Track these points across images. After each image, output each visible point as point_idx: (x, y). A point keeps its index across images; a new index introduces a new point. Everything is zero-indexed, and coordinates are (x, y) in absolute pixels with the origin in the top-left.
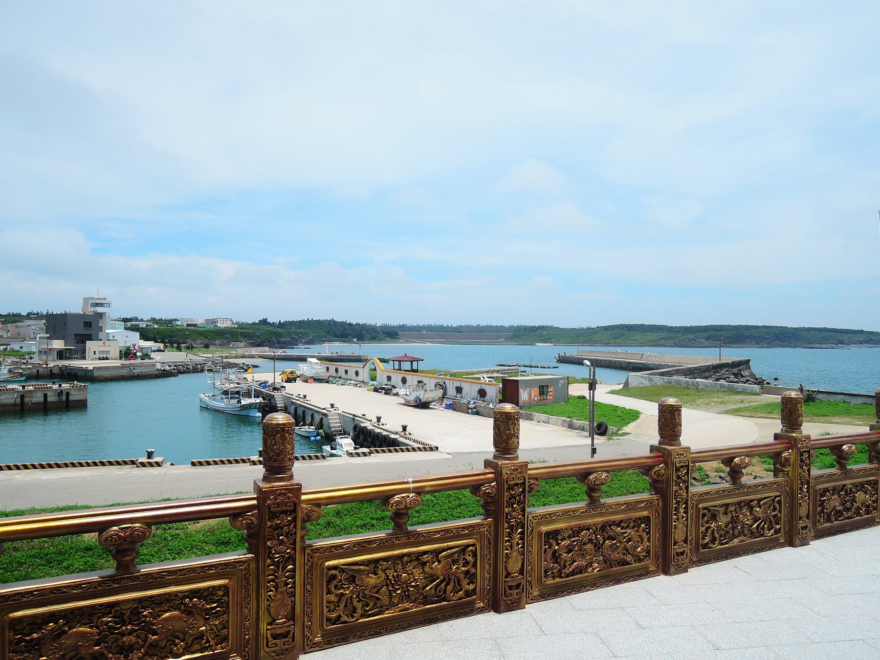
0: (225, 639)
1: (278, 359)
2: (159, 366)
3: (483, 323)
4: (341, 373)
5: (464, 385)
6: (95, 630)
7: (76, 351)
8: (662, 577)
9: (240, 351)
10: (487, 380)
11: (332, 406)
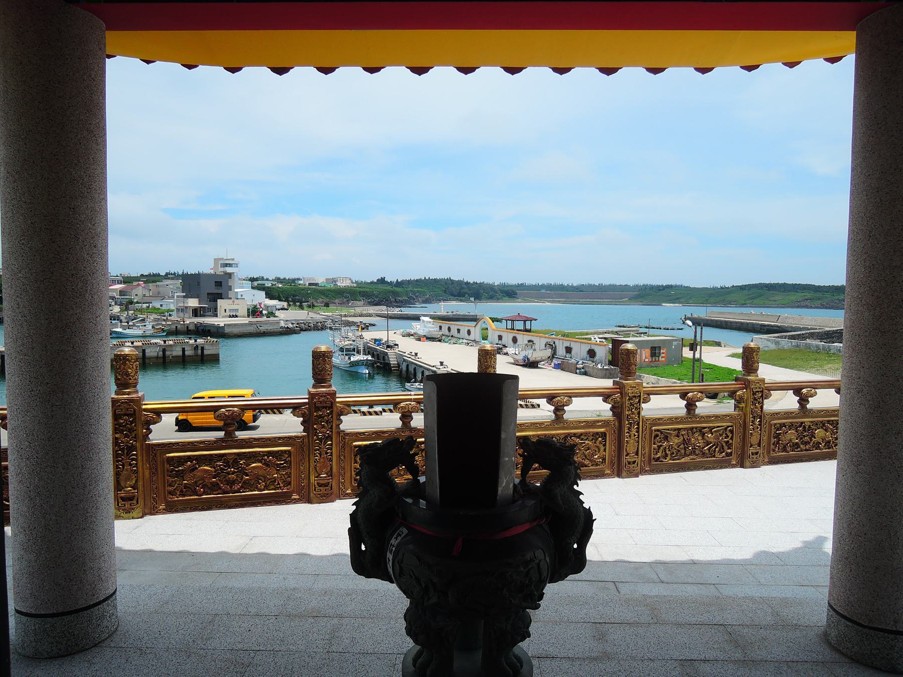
0: (290, 483)
1: (391, 318)
2: (282, 324)
3: (606, 282)
4: (454, 332)
5: (573, 345)
6: (213, 469)
7: (209, 309)
8: (616, 479)
9: (358, 310)
10: (598, 340)
11: (442, 363)
